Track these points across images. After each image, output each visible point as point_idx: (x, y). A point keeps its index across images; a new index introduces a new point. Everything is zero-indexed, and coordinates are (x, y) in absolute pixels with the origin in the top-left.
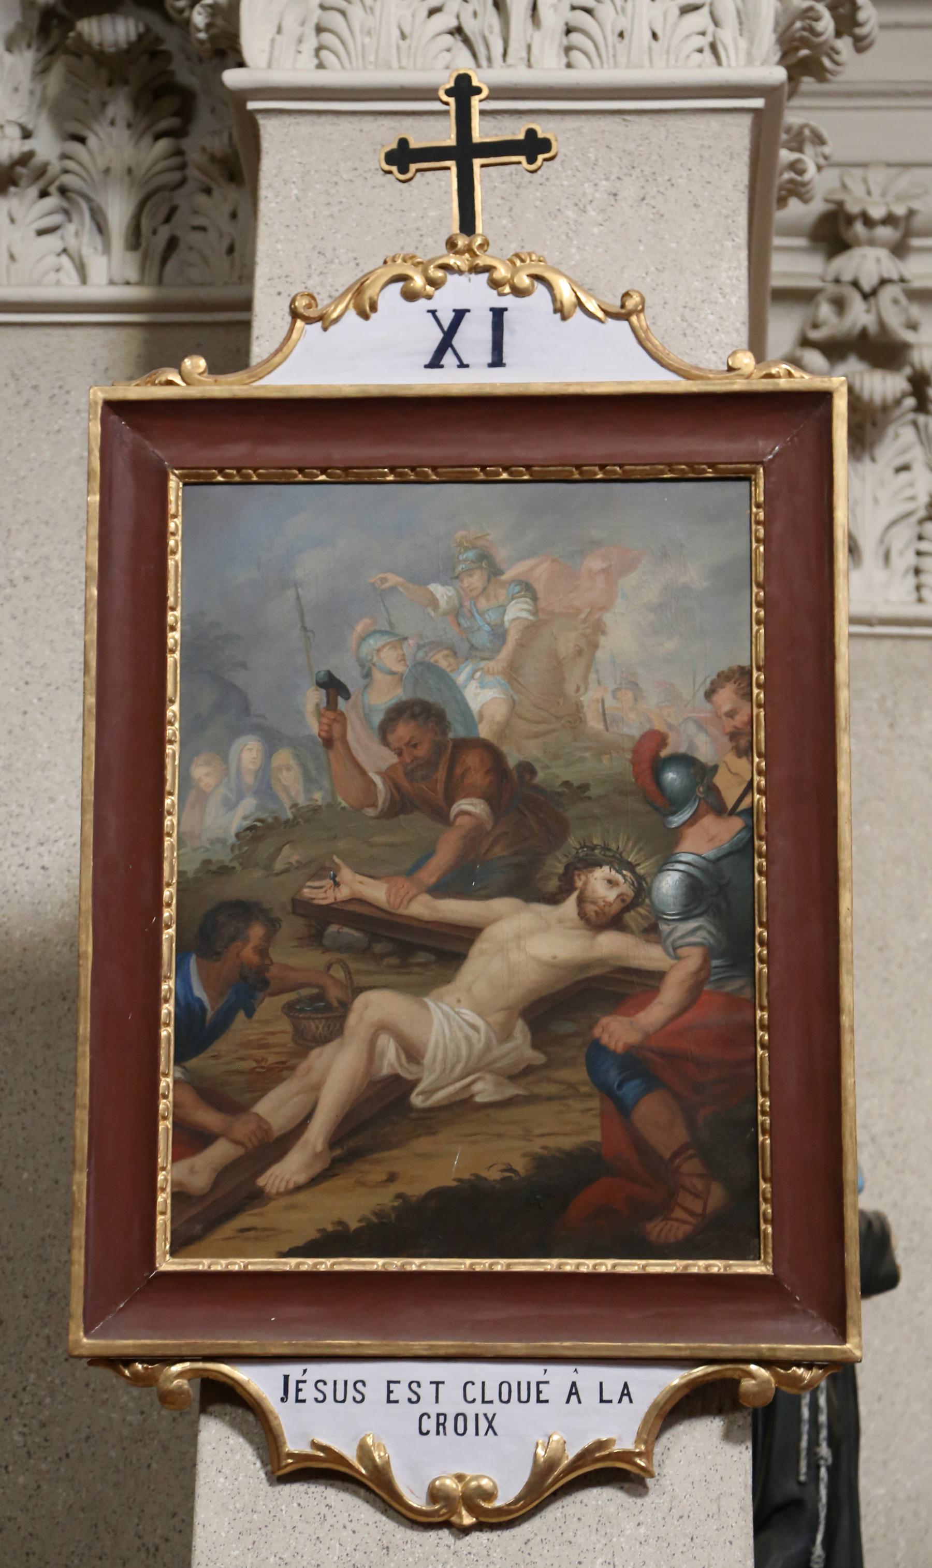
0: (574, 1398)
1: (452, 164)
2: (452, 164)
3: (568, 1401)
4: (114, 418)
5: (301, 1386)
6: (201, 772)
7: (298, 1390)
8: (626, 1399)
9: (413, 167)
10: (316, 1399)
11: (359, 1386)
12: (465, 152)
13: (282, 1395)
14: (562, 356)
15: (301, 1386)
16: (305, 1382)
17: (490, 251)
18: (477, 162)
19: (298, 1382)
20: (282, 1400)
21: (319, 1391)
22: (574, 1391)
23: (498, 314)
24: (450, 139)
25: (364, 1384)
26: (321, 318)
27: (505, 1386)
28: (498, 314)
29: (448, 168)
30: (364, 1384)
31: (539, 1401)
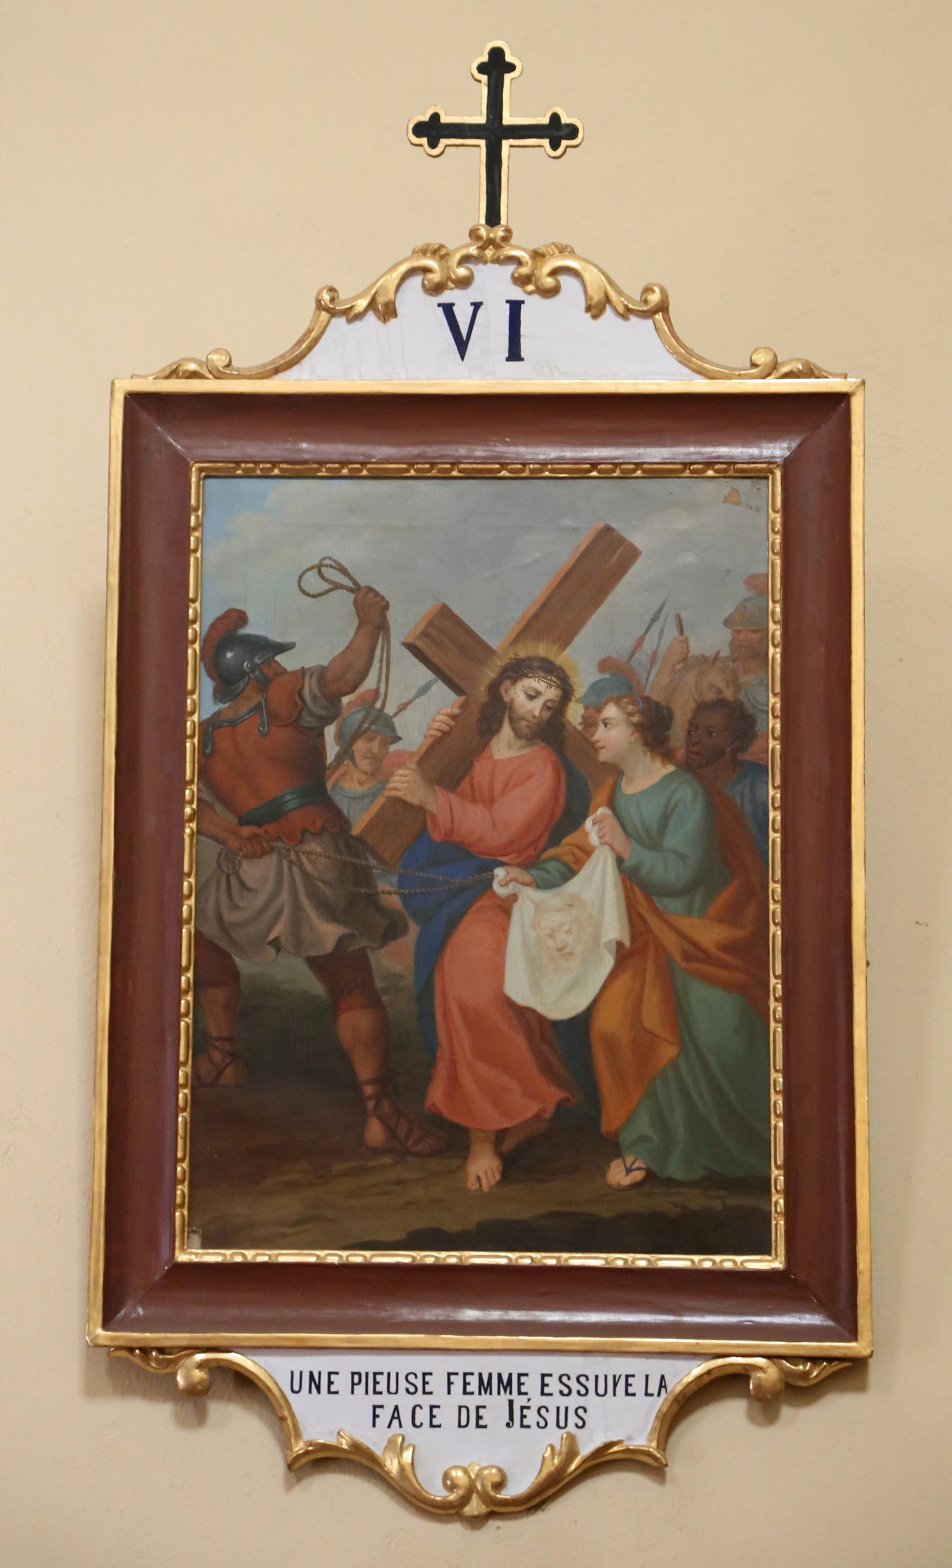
0: (396, 1422)
1: (482, 143)
2: (482, 143)
3: (389, 1426)
4: (145, 417)
5: (525, 1412)
6: (712, 1006)
7: (523, 1417)
8: (396, 1422)
9: (444, 142)
10: (576, 1425)
11: (581, 1412)
12: (494, 132)
13: (507, 1419)
14: (577, 355)
15: (525, 1412)
16: (529, 1408)
17: (513, 241)
18: (506, 144)
19: (522, 1408)
20: (508, 1425)
21: (545, 1419)
22: (396, 1415)
23: (515, 307)
24: (481, 119)
25: (585, 1411)
26: (345, 312)
27: (464, 1411)
28: (515, 307)
29: (478, 146)
30: (585, 1411)
31: (478, 1426)
